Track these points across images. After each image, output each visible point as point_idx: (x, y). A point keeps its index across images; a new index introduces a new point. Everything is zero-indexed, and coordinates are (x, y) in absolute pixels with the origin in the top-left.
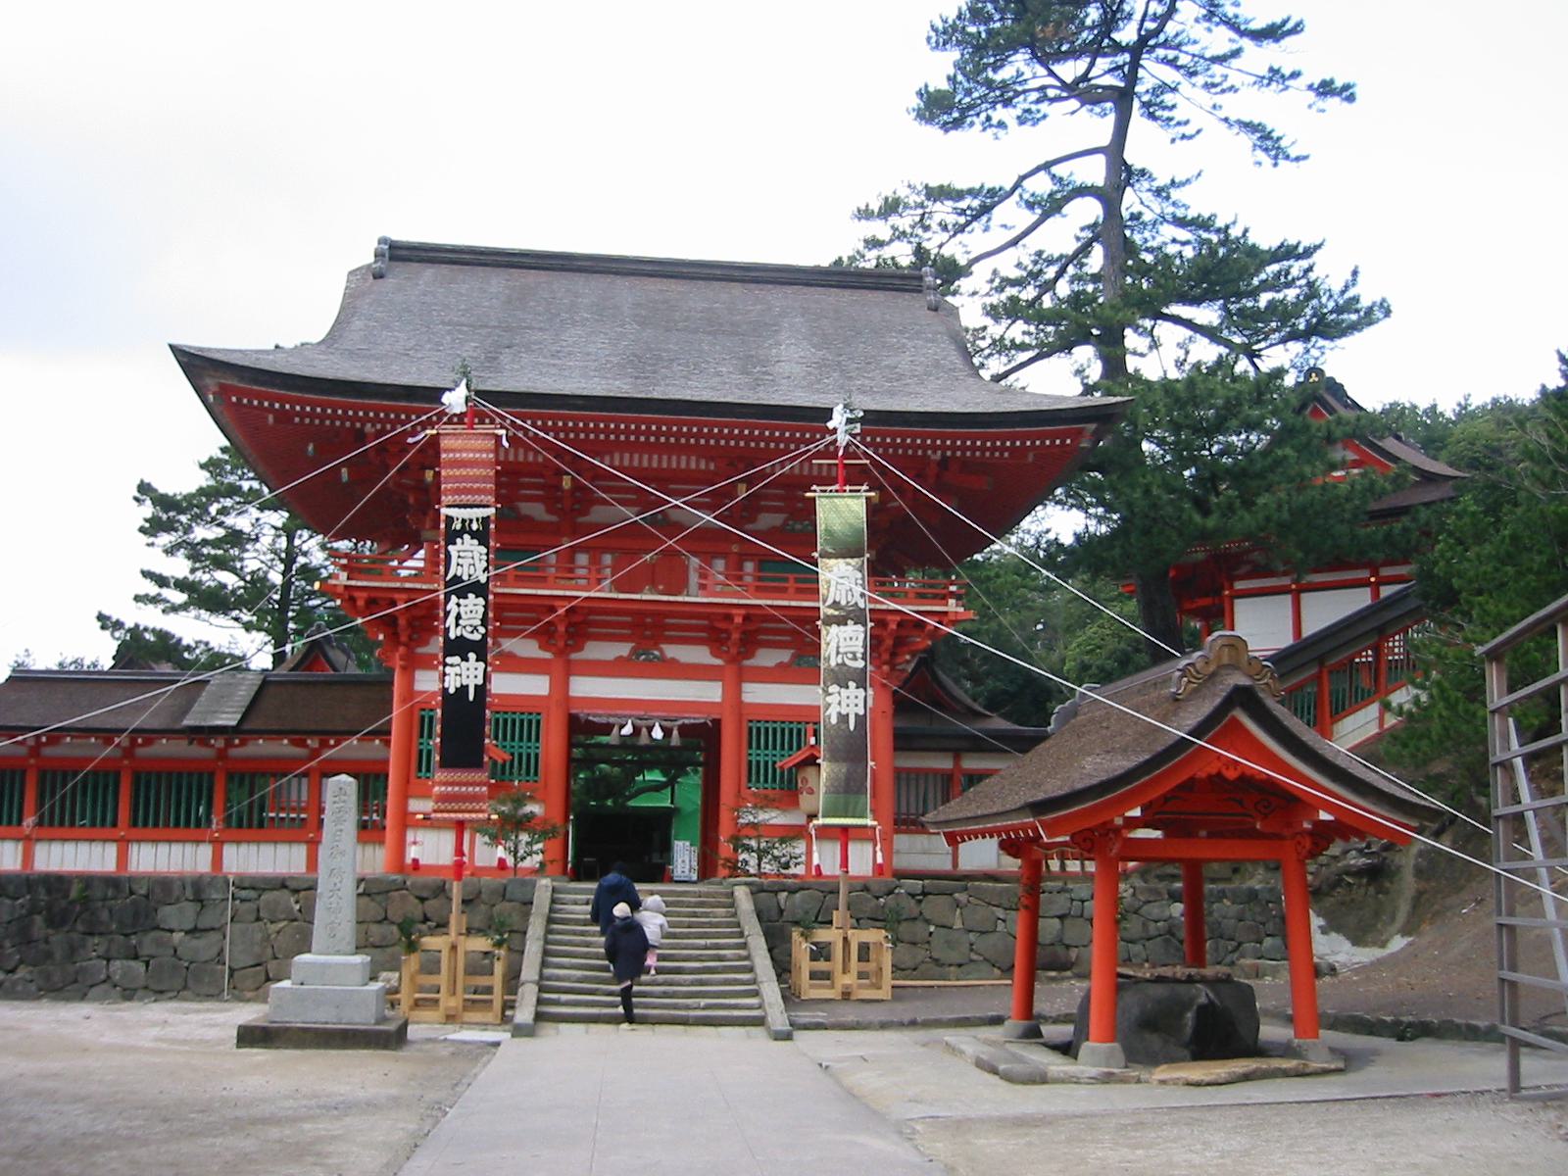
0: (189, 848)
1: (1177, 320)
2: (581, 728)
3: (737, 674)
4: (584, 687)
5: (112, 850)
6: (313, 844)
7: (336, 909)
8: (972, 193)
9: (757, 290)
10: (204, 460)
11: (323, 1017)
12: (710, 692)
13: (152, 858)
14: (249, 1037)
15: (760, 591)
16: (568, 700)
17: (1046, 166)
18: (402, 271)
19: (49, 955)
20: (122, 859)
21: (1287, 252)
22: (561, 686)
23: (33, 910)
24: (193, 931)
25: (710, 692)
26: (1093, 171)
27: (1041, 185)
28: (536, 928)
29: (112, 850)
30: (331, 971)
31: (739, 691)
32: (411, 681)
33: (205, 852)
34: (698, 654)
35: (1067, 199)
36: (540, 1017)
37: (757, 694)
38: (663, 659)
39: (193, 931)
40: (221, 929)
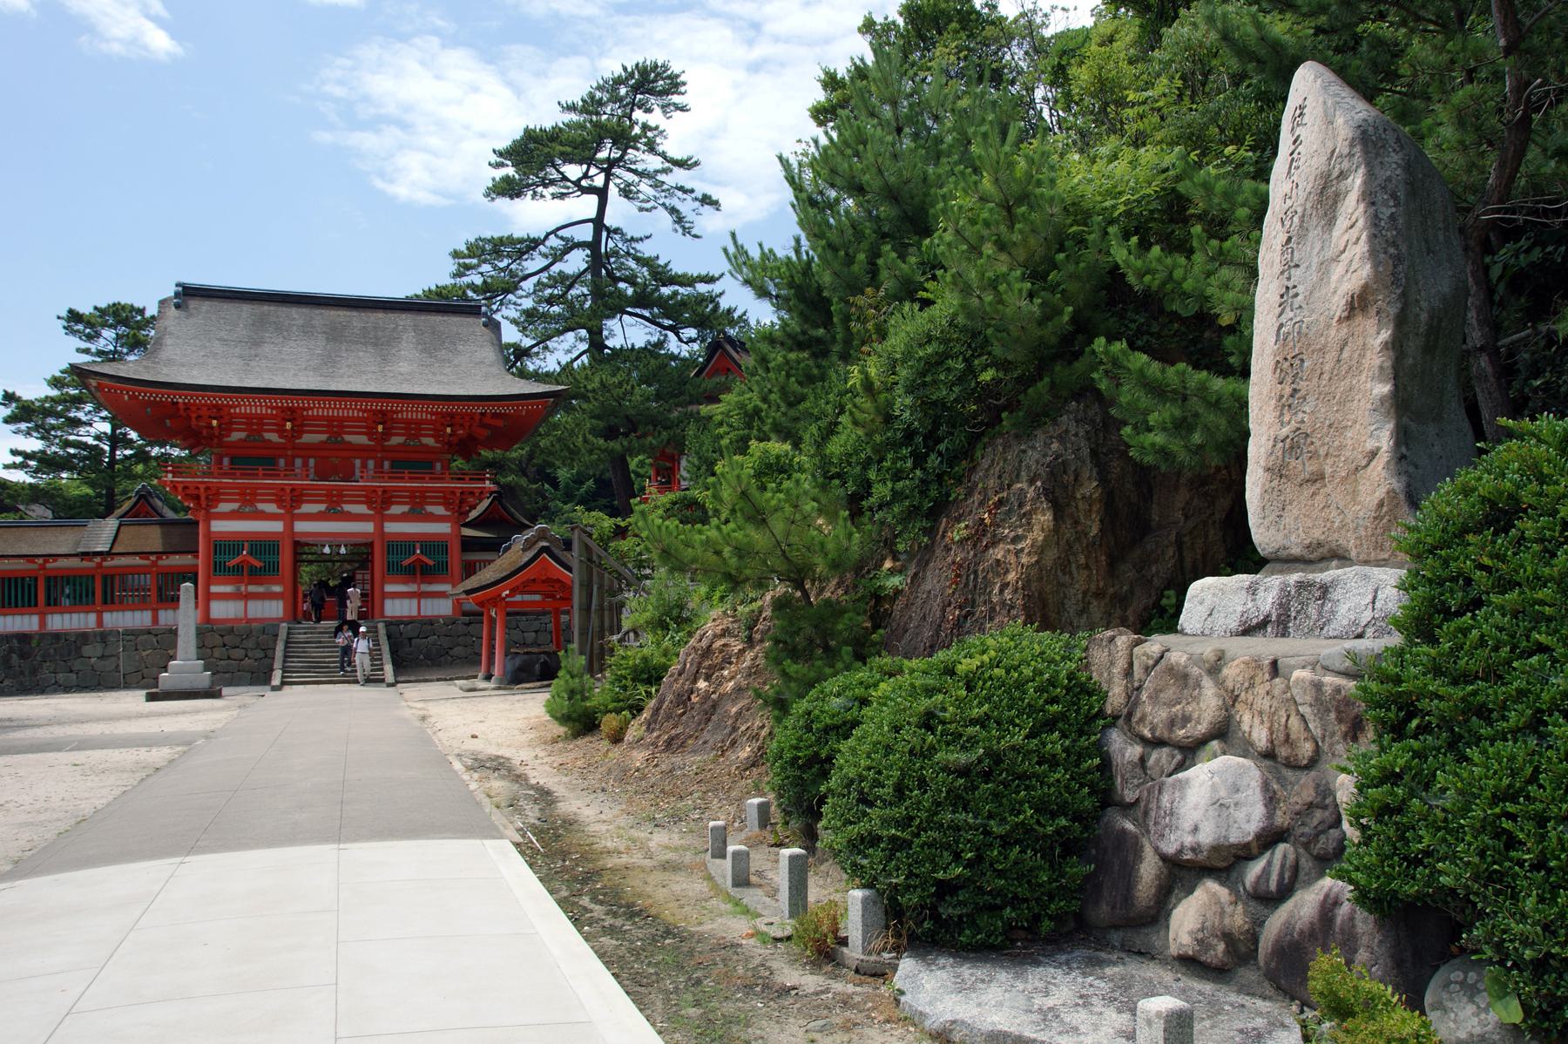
0: (82, 615)
1: (631, 314)
2: (301, 548)
3: (380, 517)
4: (301, 527)
5: (35, 619)
6: (207, 618)
7: (187, 641)
8: (521, 241)
9: (392, 316)
10: (49, 377)
11: (185, 685)
12: (369, 527)
13: (58, 622)
14: (152, 697)
15: (391, 479)
16: (293, 534)
17: (554, 232)
18: (193, 303)
19: (22, 673)
20: (43, 623)
21: (791, 179)
22: (289, 526)
23: (11, 650)
24: (102, 657)
25: (369, 527)
26: (586, 233)
27: (553, 242)
28: (280, 647)
29: (35, 619)
30: (185, 665)
31: (382, 527)
32: (209, 526)
33: (92, 617)
34: (362, 509)
35: (571, 249)
36: (283, 683)
37: (391, 527)
38: (343, 512)
39: (102, 657)
40: (117, 656)
